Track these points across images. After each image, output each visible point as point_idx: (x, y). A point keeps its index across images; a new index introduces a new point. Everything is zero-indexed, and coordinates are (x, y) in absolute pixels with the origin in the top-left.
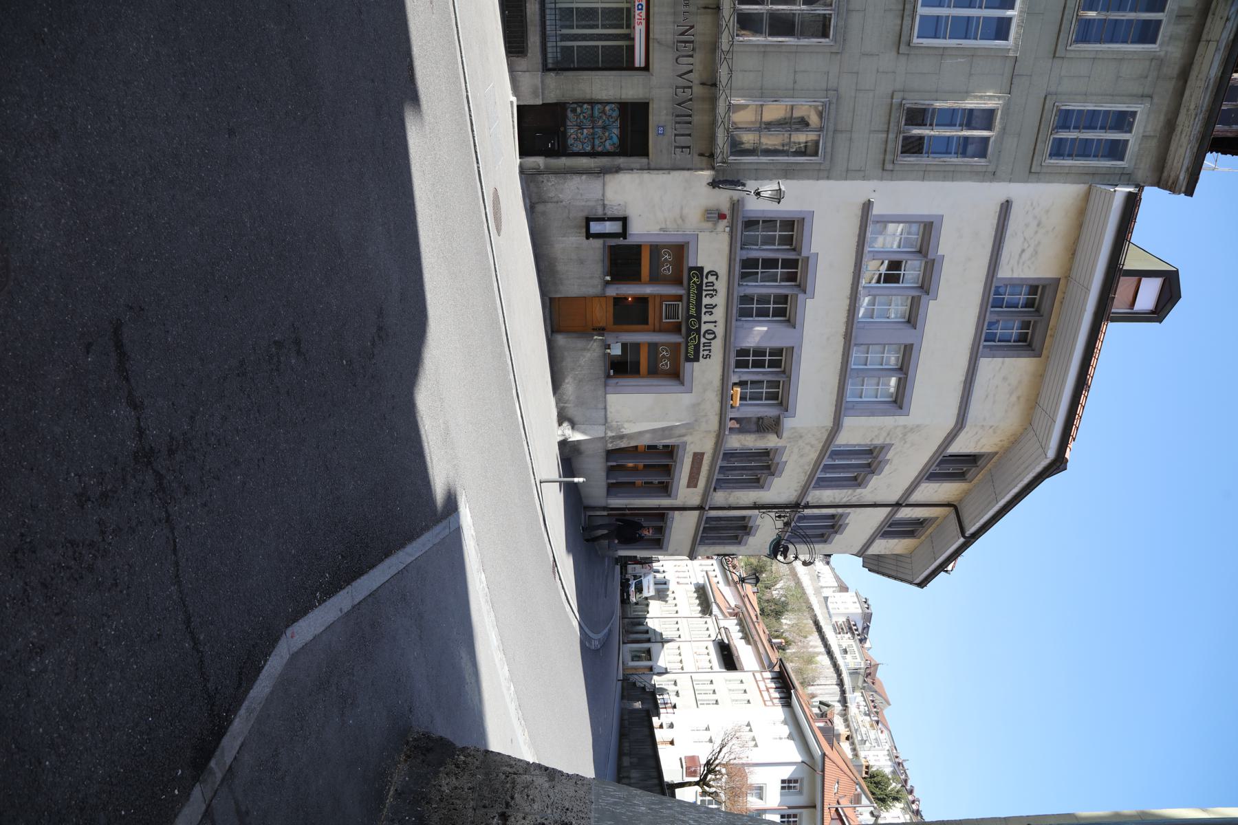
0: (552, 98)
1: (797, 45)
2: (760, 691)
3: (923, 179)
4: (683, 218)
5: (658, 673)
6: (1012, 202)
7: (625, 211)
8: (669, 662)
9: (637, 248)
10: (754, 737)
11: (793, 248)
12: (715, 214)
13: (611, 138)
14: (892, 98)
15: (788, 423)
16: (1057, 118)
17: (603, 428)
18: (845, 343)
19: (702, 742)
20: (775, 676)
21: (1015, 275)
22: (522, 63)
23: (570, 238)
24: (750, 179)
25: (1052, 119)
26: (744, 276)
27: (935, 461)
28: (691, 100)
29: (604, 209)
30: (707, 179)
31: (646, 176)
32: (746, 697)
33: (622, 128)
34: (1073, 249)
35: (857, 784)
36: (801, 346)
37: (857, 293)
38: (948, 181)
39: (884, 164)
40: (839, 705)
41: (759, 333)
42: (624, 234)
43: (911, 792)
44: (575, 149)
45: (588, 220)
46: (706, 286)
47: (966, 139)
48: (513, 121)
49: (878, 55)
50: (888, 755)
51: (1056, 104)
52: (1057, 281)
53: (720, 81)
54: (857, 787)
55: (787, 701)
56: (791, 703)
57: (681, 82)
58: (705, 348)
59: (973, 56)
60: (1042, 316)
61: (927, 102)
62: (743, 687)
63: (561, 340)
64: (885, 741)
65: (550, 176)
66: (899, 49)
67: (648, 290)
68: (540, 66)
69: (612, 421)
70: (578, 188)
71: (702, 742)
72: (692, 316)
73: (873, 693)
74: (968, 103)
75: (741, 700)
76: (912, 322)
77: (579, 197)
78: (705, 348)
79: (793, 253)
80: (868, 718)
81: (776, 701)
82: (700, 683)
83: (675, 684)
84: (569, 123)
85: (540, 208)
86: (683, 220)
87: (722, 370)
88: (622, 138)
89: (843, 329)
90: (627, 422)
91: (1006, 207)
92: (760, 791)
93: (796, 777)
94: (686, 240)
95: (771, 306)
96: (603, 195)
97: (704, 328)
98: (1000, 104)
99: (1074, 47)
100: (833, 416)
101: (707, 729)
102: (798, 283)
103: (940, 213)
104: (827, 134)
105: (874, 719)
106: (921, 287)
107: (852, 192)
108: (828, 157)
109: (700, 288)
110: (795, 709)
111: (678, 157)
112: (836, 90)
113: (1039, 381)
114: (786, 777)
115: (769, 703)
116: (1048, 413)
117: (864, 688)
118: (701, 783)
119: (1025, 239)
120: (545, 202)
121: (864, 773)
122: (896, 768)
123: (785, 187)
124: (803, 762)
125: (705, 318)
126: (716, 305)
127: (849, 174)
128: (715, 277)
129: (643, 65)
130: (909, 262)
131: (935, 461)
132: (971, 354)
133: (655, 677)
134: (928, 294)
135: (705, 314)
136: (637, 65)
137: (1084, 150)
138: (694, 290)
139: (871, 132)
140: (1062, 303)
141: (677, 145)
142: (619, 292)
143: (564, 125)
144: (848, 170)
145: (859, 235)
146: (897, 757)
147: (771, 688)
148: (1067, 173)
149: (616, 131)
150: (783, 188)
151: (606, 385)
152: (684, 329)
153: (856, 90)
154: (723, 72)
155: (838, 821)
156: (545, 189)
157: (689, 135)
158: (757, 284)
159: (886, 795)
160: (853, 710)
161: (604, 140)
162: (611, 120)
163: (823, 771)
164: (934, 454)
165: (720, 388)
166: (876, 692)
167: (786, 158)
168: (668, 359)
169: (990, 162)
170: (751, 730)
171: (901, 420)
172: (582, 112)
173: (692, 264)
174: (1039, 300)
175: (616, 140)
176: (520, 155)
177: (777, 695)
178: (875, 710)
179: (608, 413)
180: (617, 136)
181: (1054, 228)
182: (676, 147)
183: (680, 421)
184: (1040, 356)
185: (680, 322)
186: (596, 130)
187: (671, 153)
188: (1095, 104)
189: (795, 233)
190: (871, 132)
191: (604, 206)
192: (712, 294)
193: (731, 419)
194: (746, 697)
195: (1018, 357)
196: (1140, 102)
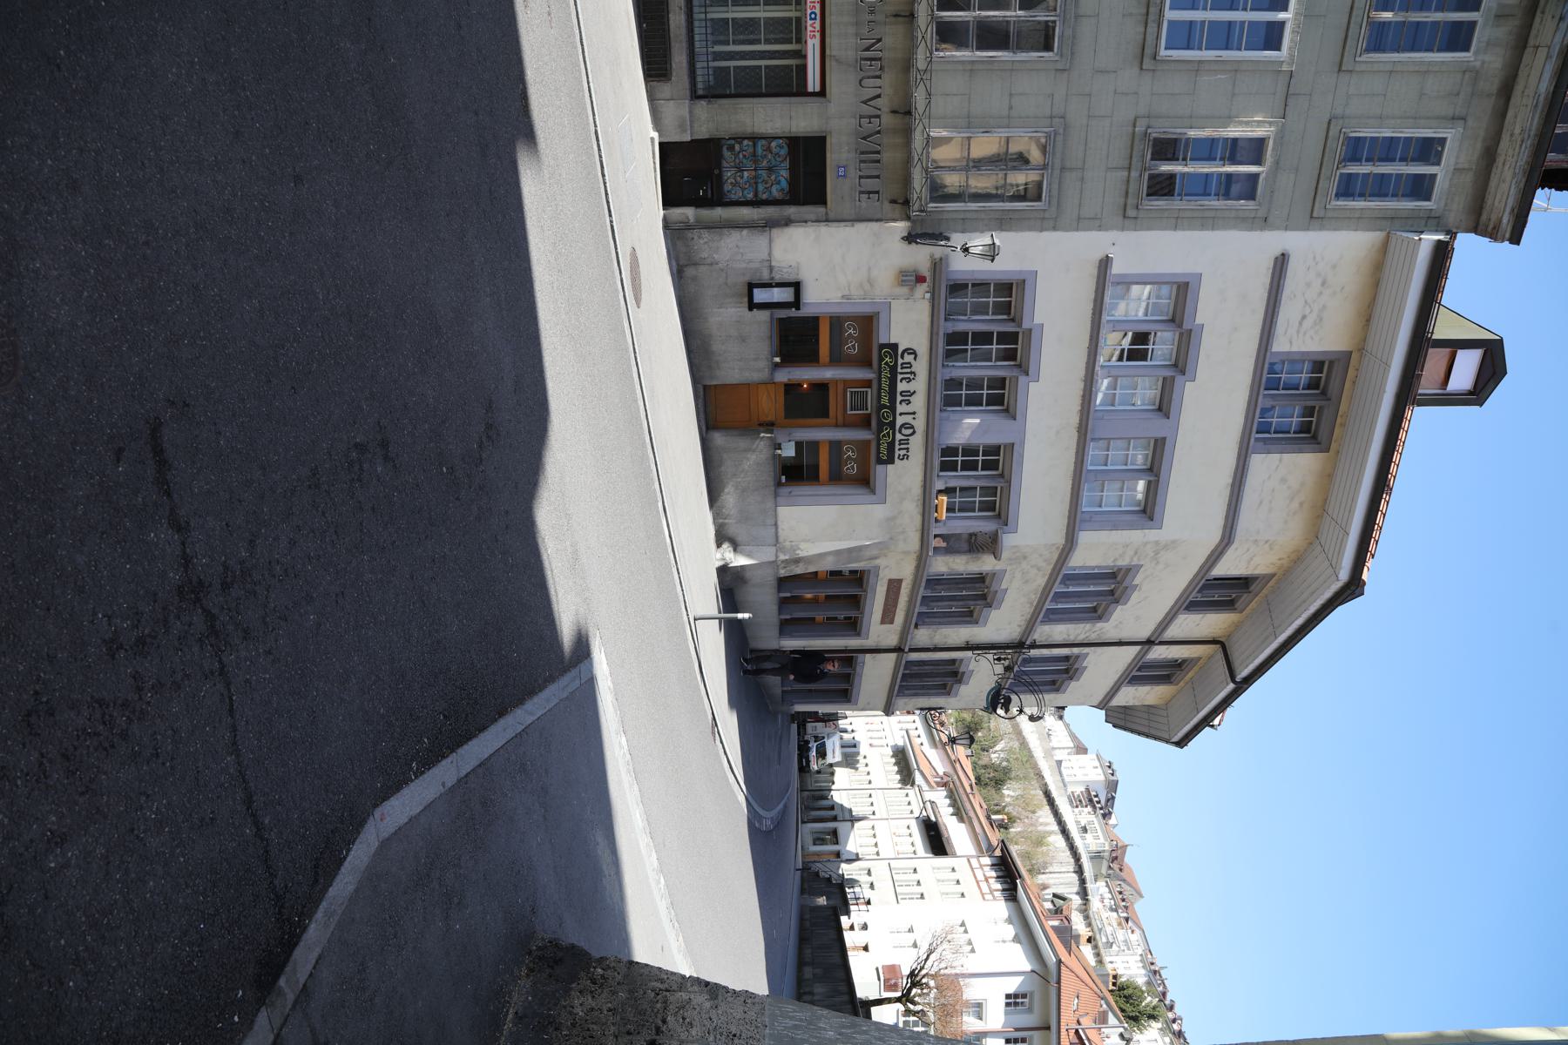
0: (703, 132)
1: (1013, 61)
2: (977, 882)
3: (1175, 228)
4: (870, 282)
6: (1289, 256)
7: (798, 274)
9: (814, 321)
10: (970, 940)
12: (911, 276)
13: (779, 183)
14: (1135, 127)
15: (1008, 541)
16: (1344, 148)
17: (773, 549)
18: (1079, 437)
21: (1295, 349)
22: (665, 89)
24: (956, 232)
25: (1339, 149)
26: (949, 355)
28: (879, 132)
31: (825, 230)
32: (959, 889)
33: (793, 170)
34: (1368, 313)
35: (1102, 999)
39: (1125, 210)
41: (969, 427)
42: (796, 303)
43: (1171, 1008)
44: (734, 197)
46: (902, 368)
48: (654, 163)
51: (1344, 130)
53: (916, 109)
54: (1103, 1002)
55: (1011, 894)
57: (867, 110)
58: (902, 446)
59: (1236, 71)
61: (1179, 131)
63: (719, 438)
67: (827, 374)
72: (885, 407)
73: (1119, 883)
77: (739, 257)
78: (902, 446)
79: (1013, 324)
80: (1115, 914)
81: (998, 894)
83: (869, 873)
85: (690, 272)
86: (871, 285)
88: (793, 182)
92: (978, 1009)
93: (1023, 990)
96: (770, 254)
97: (900, 421)
98: (1271, 131)
99: (1365, 57)
101: (911, 930)
102: (1018, 363)
106: (1175, 365)
107: (1086, 245)
108: (1054, 201)
113: (1328, 479)
114: (1011, 991)
115: (989, 897)
117: (1109, 876)
118: (904, 999)
119: (1306, 302)
121: (1111, 983)
122: (1152, 978)
124: (1032, 971)
125: (900, 408)
126: (915, 392)
127: (1081, 223)
128: (913, 356)
129: (818, 89)
132: (1240, 449)
133: (844, 866)
135: (900, 403)
136: (810, 89)
137: (1380, 187)
138: (886, 373)
139: (1108, 169)
140: (1354, 382)
143: (719, 166)
145: (1095, 300)
146: (1152, 964)
149: (785, 173)
150: (997, 242)
151: (776, 495)
154: (919, 96)
157: (878, 177)
158: (966, 364)
159: (1139, 1012)
160: (1095, 904)
163: (1059, 982)
166: (1124, 881)
167: (1001, 204)
170: (966, 932)
171: (1152, 535)
173: (883, 341)
175: (784, 184)
177: (999, 886)
178: (1124, 904)
179: (780, 530)
181: (1343, 288)
182: (861, 192)
184: (1327, 450)
185: (869, 416)
186: (760, 172)
189: (1013, 299)
191: (771, 268)
193: (936, 536)
194: (959, 889)
195: (1301, 451)
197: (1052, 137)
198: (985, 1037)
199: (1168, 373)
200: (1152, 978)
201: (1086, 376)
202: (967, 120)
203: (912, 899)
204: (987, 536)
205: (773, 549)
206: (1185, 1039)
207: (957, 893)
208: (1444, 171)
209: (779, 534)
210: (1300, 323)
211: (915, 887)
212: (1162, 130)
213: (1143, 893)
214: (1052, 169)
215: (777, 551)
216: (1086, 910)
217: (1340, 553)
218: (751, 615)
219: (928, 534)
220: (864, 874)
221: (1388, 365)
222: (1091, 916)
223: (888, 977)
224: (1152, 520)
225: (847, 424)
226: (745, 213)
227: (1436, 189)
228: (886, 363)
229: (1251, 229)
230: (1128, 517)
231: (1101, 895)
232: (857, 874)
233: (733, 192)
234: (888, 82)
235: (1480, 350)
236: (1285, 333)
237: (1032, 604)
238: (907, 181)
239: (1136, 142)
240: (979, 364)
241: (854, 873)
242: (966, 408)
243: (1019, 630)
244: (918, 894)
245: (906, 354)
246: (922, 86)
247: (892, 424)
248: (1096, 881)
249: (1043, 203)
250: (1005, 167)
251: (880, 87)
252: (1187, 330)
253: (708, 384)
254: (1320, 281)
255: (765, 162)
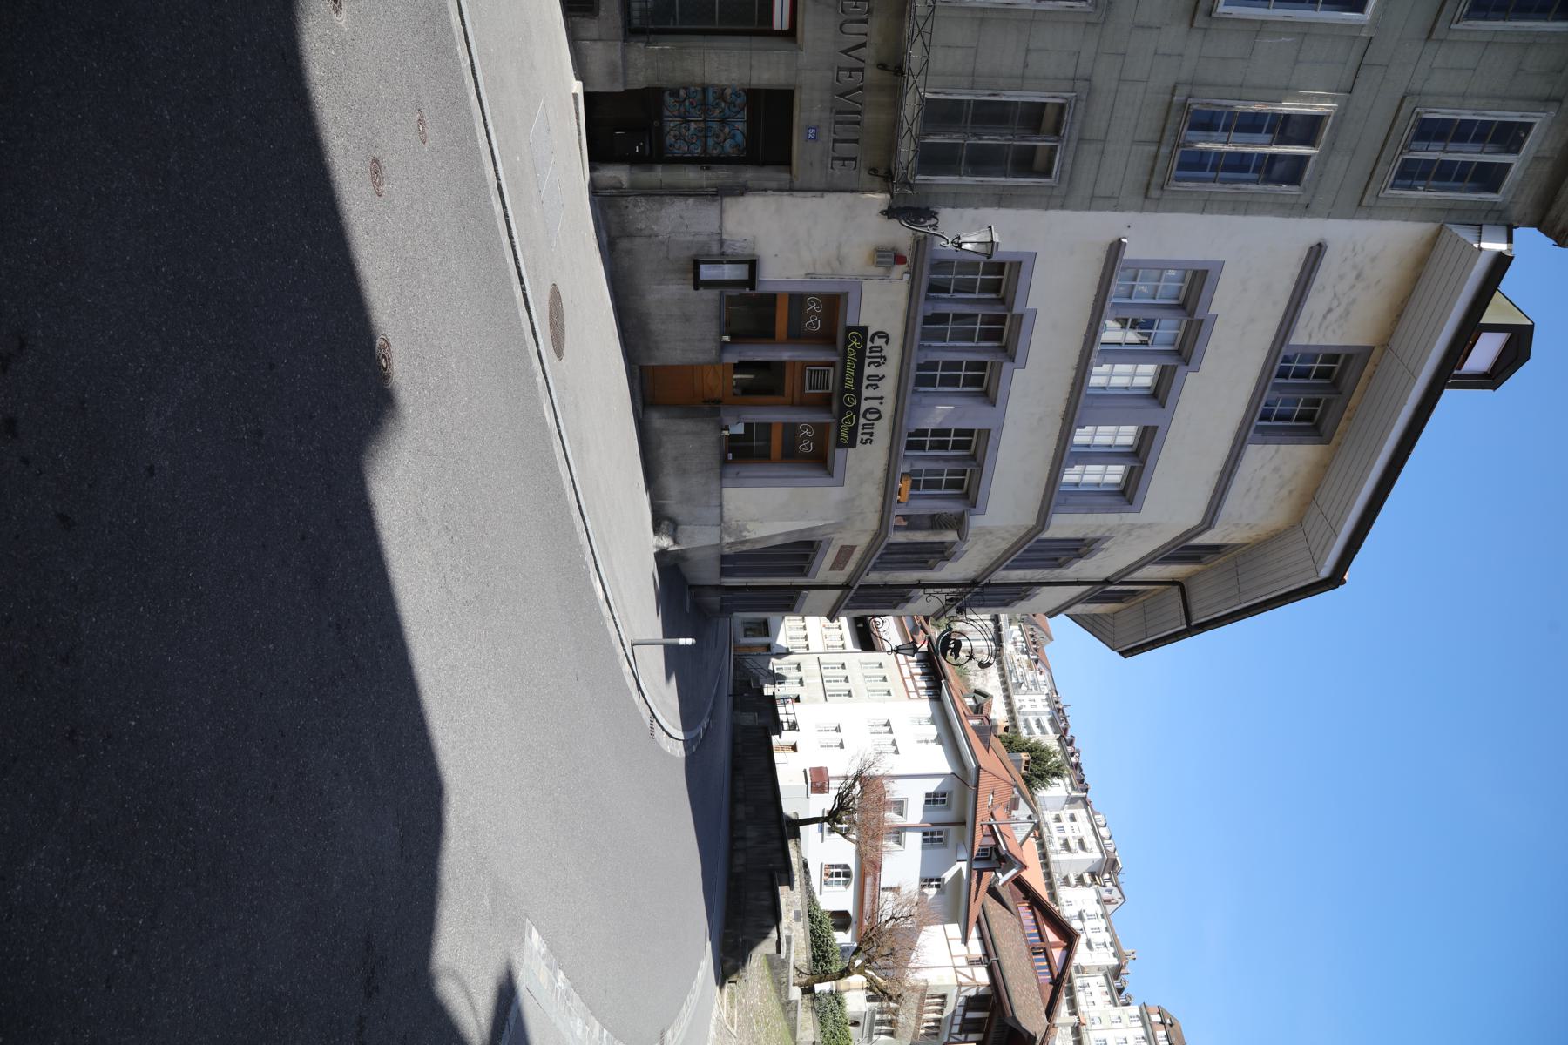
0: (639, 80)
1: (1035, 10)
2: (903, 679)
3: (1203, 211)
4: (840, 260)
5: (778, 654)
6: (1327, 247)
7: (754, 249)
8: (791, 639)
9: (771, 299)
10: (894, 740)
11: (1000, 297)
12: (889, 256)
13: (733, 137)
14: (1173, 94)
15: (975, 522)
16: (1413, 130)
17: (717, 530)
18: (1063, 426)
19: (831, 746)
20: (922, 659)
21: (1313, 342)
22: (591, 27)
23: (670, 286)
24: (946, 207)
25: (1406, 129)
26: (926, 336)
27: (1161, 555)
28: (860, 88)
29: (722, 246)
30: (880, 205)
31: (787, 200)
32: (886, 686)
33: (751, 122)
34: (1399, 310)
35: (1015, 787)
36: (1000, 429)
37: (1087, 364)
38: (1238, 214)
39: (1148, 189)
40: (990, 623)
41: (941, 413)
42: (751, 281)
43: (1071, 743)
44: (678, 153)
45: (697, 264)
46: (870, 352)
47: (1273, 157)
48: (578, 125)
49: (1160, 28)
50: (1047, 700)
51: (1418, 110)
52: (1369, 350)
53: (910, 68)
54: (1015, 789)
55: (935, 693)
56: (940, 695)
57: (846, 61)
58: (866, 431)
59: (1305, 34)
60: (1340, 393)
61: (1225, 102)
62: (881, 672)
63: (657, 420)
64: (1044, 683)
65: (638, 199)
66: (1193, 18)
67: (785, 355)
68: (620, 32)
69: (731, 520)
70: (681, 217)
71: (831, 746)
72: (848, 391)
73: (1031, 627)
74: (1288, 106)
75: (875, 677)
76: (1160, 397)
77: (683, 229)
78: (866, 431)
79: (1002, 307)
80: (1025, 657)
81: (922, 692)
82: (830, 666)
83: (799, 668)
84: (667, 113)
85: (624, 244)
86: (840, 263)
87: (887, 456)
88: (751, 136)
89: (1063, 408)
90: (751, 520)
91: (1317, 252)
92: (900, 807)
93: (944, 790)
94: (845, 289)
95: (963, 373)
96: (721, 227)
97: (865, 405)
98: (1333, 108)
99: (1463, 25)
100: (1037, 513)
101: (838, 730)
102: (1003, 344)
103: (1221, 259)
104: (1067, 145)
105: (1032, 657)
106: (1178, 352)
107: (1100, 226)
108: (1066, 177)
109: (861, 355)
110: (946, 704)
111: (837, 173)
112: (1088, 80)
113: (1321, 474)
114: (931, 790)
115: (914, 695)
116: (1329, 518)
117: (1022, 620)
118: (831, 819)
119: (1335, 295)
120: (630, 236)
121: (1023, 768)
122: (1055, 715)
123: (1000, 237)
124: (953, 774)
125: (866, 393)
126: (884, 377)
127: (1093, 202)
128: (884, 340)
129: (786, 27)
130: (1163, 321)
131: (1161, 555)
132: (1236, 439)
133: (773, 660)
134: (1188, 364)
135: (867, 387)
136: (777, 26)
137: (1445, 174)
138: (852, 357)
139: (1134, 142)
140: (1371, 377)
141: (837, 155)
142: (742, 359)
143: (660, 116)
144: (1093, 197)
145: (1100, 287)
146: (1057, 702)
147: (917, 674)
148: (1412, 208)
149: (741, 126)
150: (996, 239)
151: (722, 476)
152: (835, 407)
153: (1120, 80)
154: (915, 54)
155: (991, 838)
156: (631, 217)
157: (856, 141)
158: (944, 344)
160: (1009, 648)
161: (721, 139)
162: (734, 110)
163: (977, 786)
164: (1168, 543)
165: (883, 480)
166: (1036, 625)
167: (1003, 179)
168: (812, 439)
169: (1304, 190)
170: (890, 732)
171: (1129, 518)
172: (688, 97)
173: (851, 322)
174: (1338, 373)
175: (740, 138)
176: (590, 160)
177: (924, 684)
179: (725, 510)
180: (743, 134)
181: (1379, 281)
182: (834, 159)
183: (825, 520)
184: (1328, 442)
185: (830, 395)
186: (711, 124)
187: (827, 167)
188: (1474, 112)
189: (1005, 277)
190: (1134, 142)
191: (722, 242)
192: (878, 362)
193: (896, 516)
194: (886, 686)
195: (1300, 443)
196: (1542, 109)
197: (1072, 105)
198: (905, 831)
199: (1169, 361)
200: (1055, 715)
201: (1079, 364)
202: (971, 79)
203: (840, 695)
204: (953, 517)
205: (717, 530)
206: (1081, 770)
207: (880, 677)
208: (1521, 161)
209: (724, 514)
210: (1325, 317)
211: (841, 670)
212: (1205, 101)
213: (1054, 637)
214: (1068, 141)
215: (721, 532)
216: (999, 656)
217: (1325, 550)
218: (694, 641)
219: (890, 512)
220: (794, 668)
221: (1414, 376)
222: (1004, 661)
223: (814, 781)
224: (1131, 504)
225: (804, 403)
226: (691, 176)
227: (1507, 180)
228: (854, 347)
229: (1289, 216)
230: (1107, 500)
231: (1014, 639)
232: (786, 669)
233: (677, 146)
234: (875, 30)
235: (1507, 334)
236: (1306, 327)
237: (991, 559)
238: (892, 149)
239: (1172, 113)
240: (958, 344)
241: (783, 667)
242: (940, 389)
243: (974, 574)
244: (839, 663)
245: (876, 337)
246: (919, 41)
247: (856, 409)
248: (1010, 624)
249: (1052, 180)
250: (1011, 137)
251: (866, 34)
252: (1199, 320)
253: (645, 364)
254: (1355, 273)
255: (717, 111)
